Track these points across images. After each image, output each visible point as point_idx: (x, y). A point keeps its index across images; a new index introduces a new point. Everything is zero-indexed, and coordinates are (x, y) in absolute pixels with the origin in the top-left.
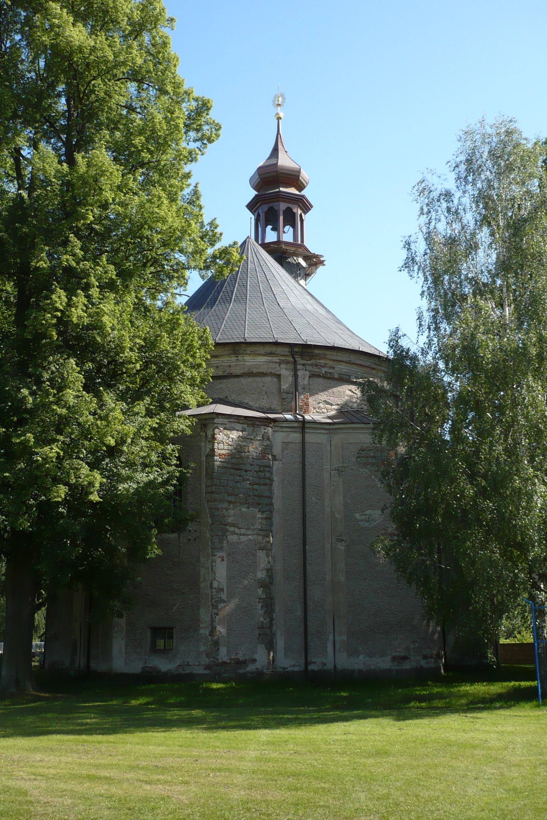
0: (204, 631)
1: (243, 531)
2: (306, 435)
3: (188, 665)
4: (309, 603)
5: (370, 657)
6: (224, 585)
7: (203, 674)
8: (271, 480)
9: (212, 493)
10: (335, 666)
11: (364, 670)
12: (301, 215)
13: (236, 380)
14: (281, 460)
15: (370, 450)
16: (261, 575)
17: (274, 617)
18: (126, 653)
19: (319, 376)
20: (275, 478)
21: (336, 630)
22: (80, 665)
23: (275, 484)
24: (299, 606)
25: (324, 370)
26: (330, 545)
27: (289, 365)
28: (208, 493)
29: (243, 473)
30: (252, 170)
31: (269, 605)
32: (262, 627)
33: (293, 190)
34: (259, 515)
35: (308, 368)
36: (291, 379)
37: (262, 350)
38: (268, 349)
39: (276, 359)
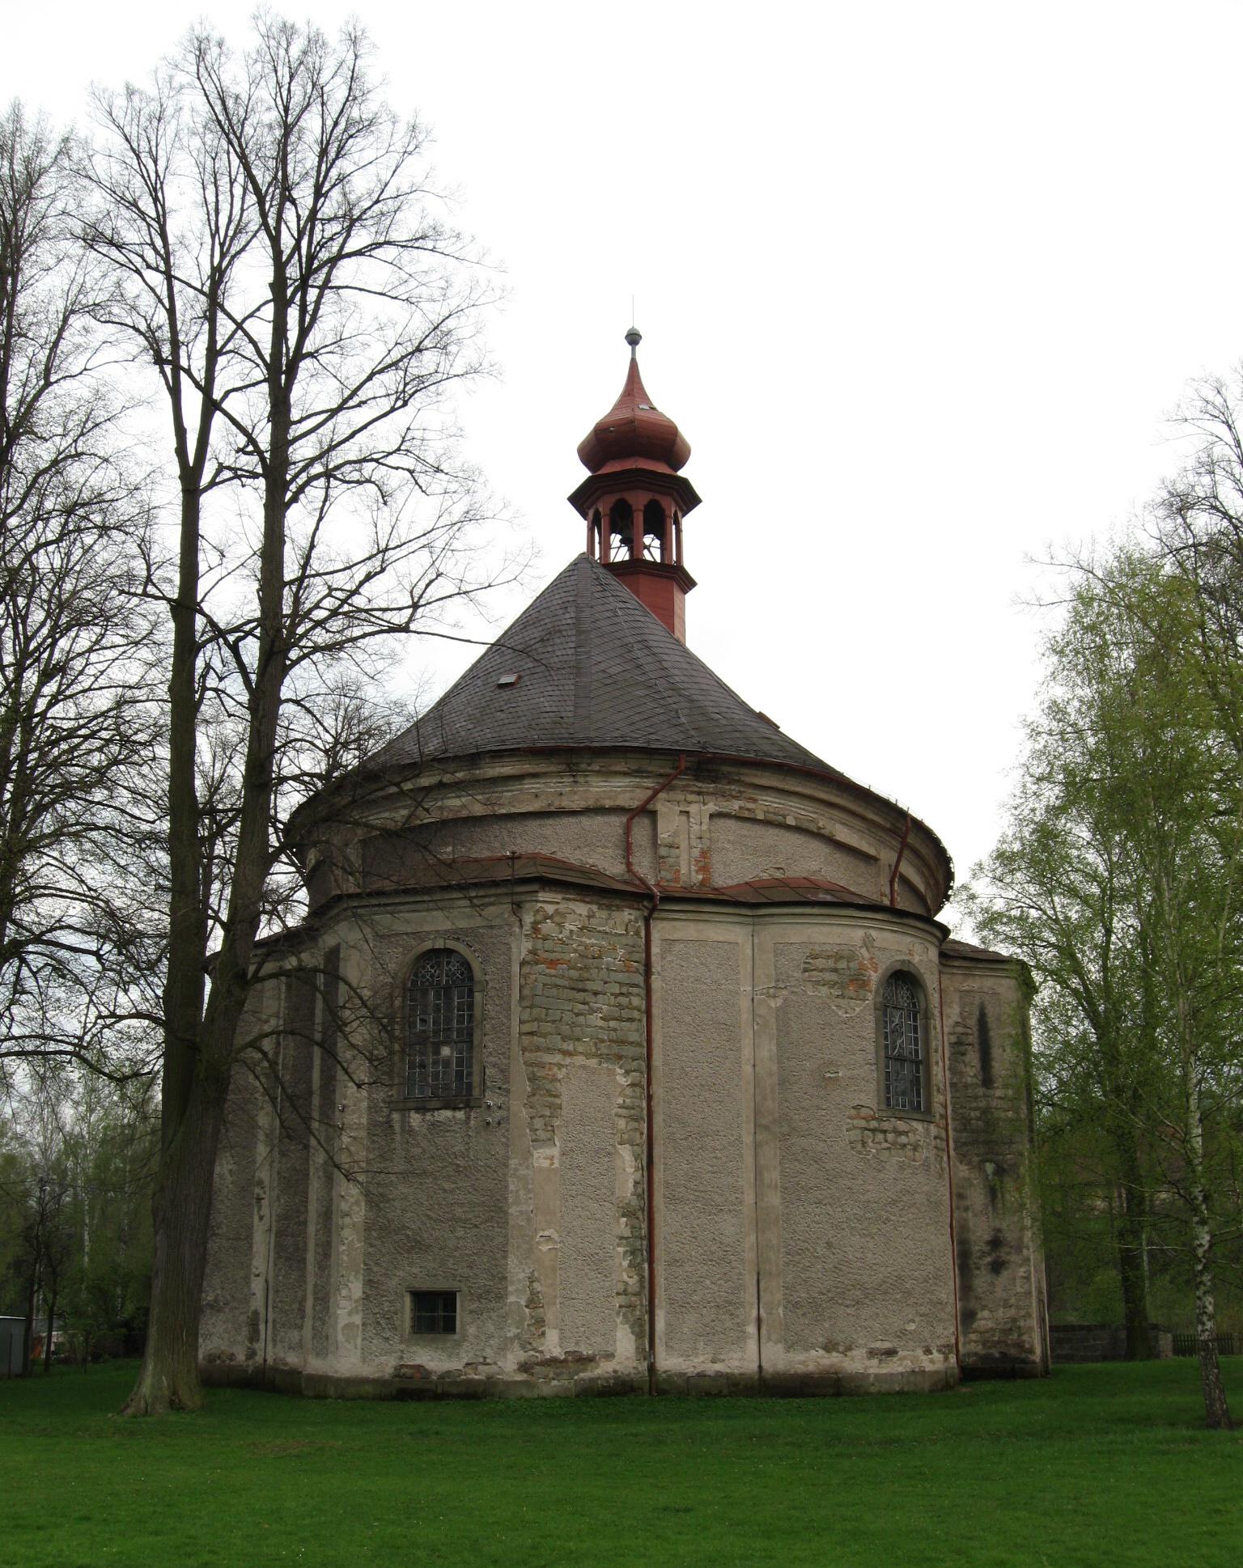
0: (516, 1298)
12: (676, 514)
13: (572, 820)
15: (829, 957)
18: (364, 1339)
29: (589, 997)
30: (583, 430)
32: (625, 1293)
33: (662, 468)
34: (623, 1081)
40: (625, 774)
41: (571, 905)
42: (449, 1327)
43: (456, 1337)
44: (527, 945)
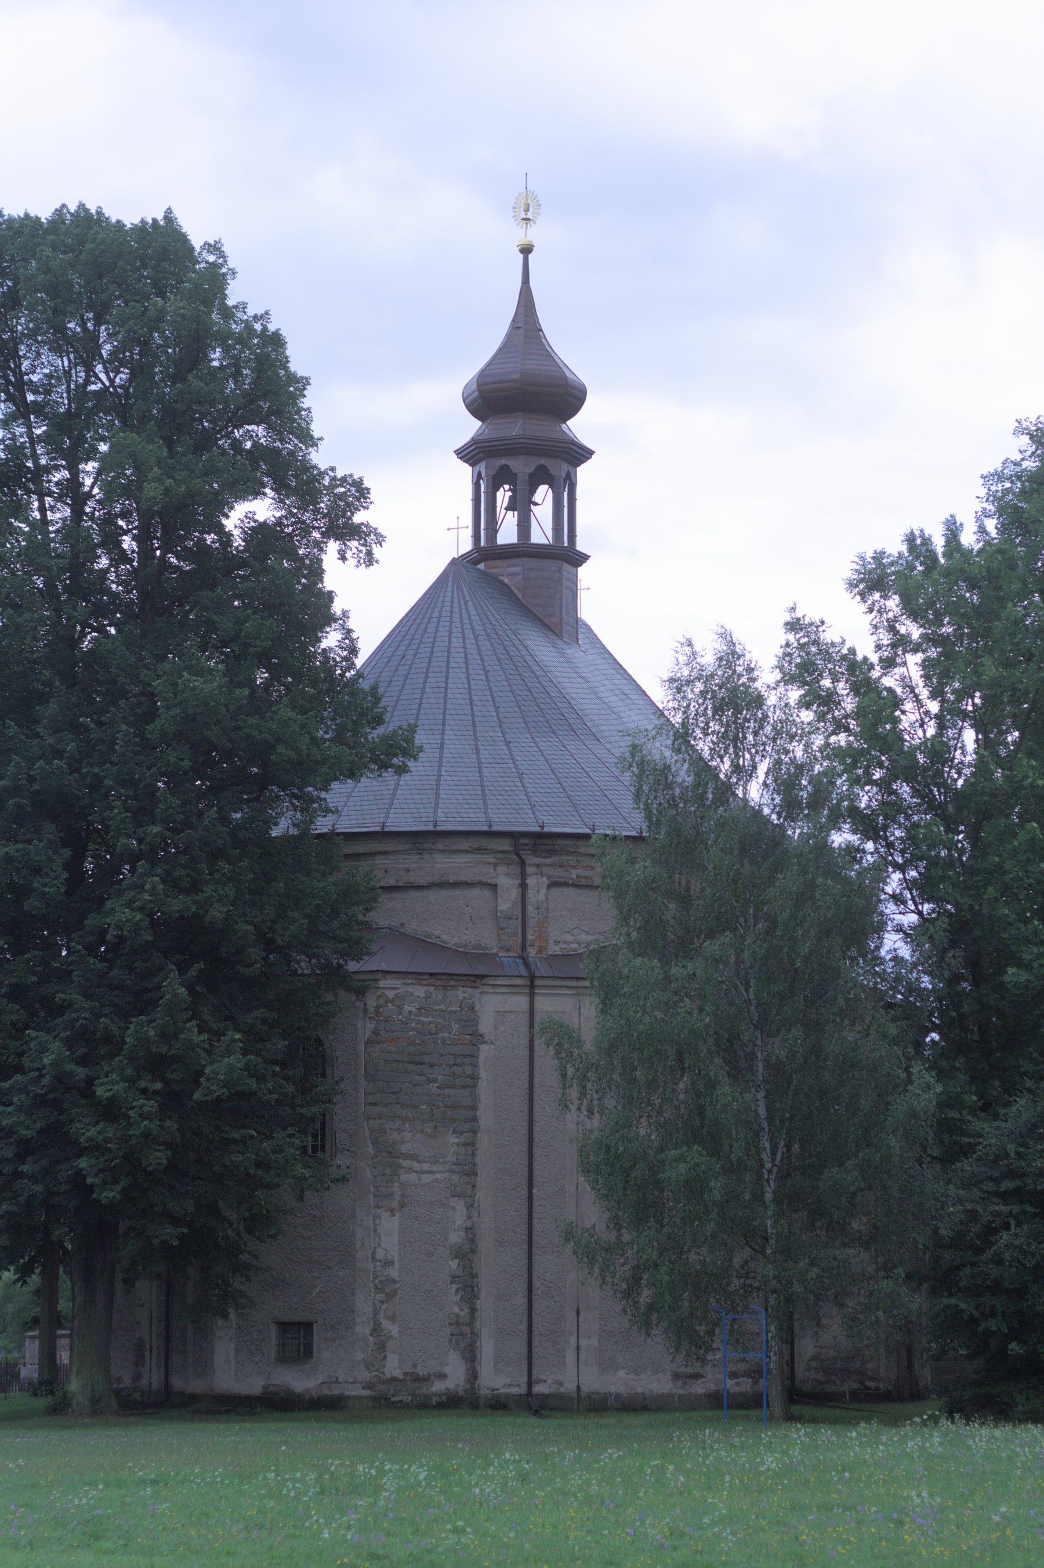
0: (363, 1329)
1: (426, 1166)
2: (538, 1000)
3: (337, 1382)
4: (536, 1283)
5: (636, 1374)
6: (395, 1255)
7: (361, 1397)
8: (475, 1078)
9: (375, 1104)
10: (578, 1388)
11: (626, 1395)
13: (419, 893)
14: (492, 1043)
16: (455, 1238)
17: (478, 1306)
18: (237, 1362)
19: (565, 884)
20: (483, 1074)
21: (581, 1329)
22: (150, 1384)
23: (482, 1084)
24: (519, 1289)
25: (574, 874)
26: (574, 1187)
27: (511, 867)
28: (369, 1104)
31: (468, 1287)
32: (457, 1323)
35: (545, 870)
36: (515, 893)
37: (465, 845)
38: (475, 843)
39: (490, 858)
40: (467, 852)
41: (410, 989)
42: (309, 1353)
43: (314, 1360)
44: (371, 1026)
